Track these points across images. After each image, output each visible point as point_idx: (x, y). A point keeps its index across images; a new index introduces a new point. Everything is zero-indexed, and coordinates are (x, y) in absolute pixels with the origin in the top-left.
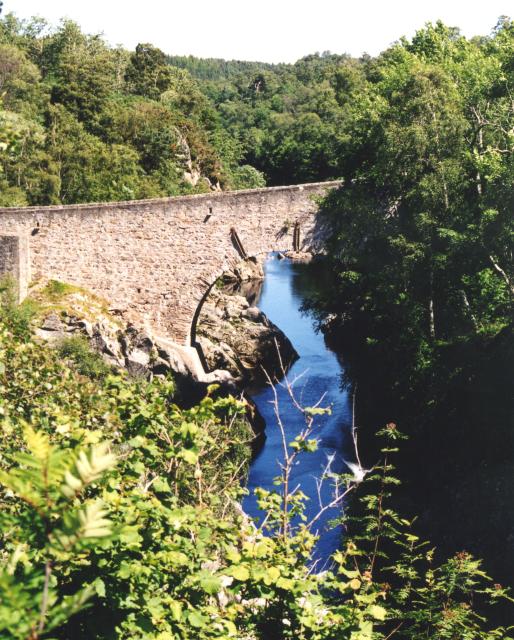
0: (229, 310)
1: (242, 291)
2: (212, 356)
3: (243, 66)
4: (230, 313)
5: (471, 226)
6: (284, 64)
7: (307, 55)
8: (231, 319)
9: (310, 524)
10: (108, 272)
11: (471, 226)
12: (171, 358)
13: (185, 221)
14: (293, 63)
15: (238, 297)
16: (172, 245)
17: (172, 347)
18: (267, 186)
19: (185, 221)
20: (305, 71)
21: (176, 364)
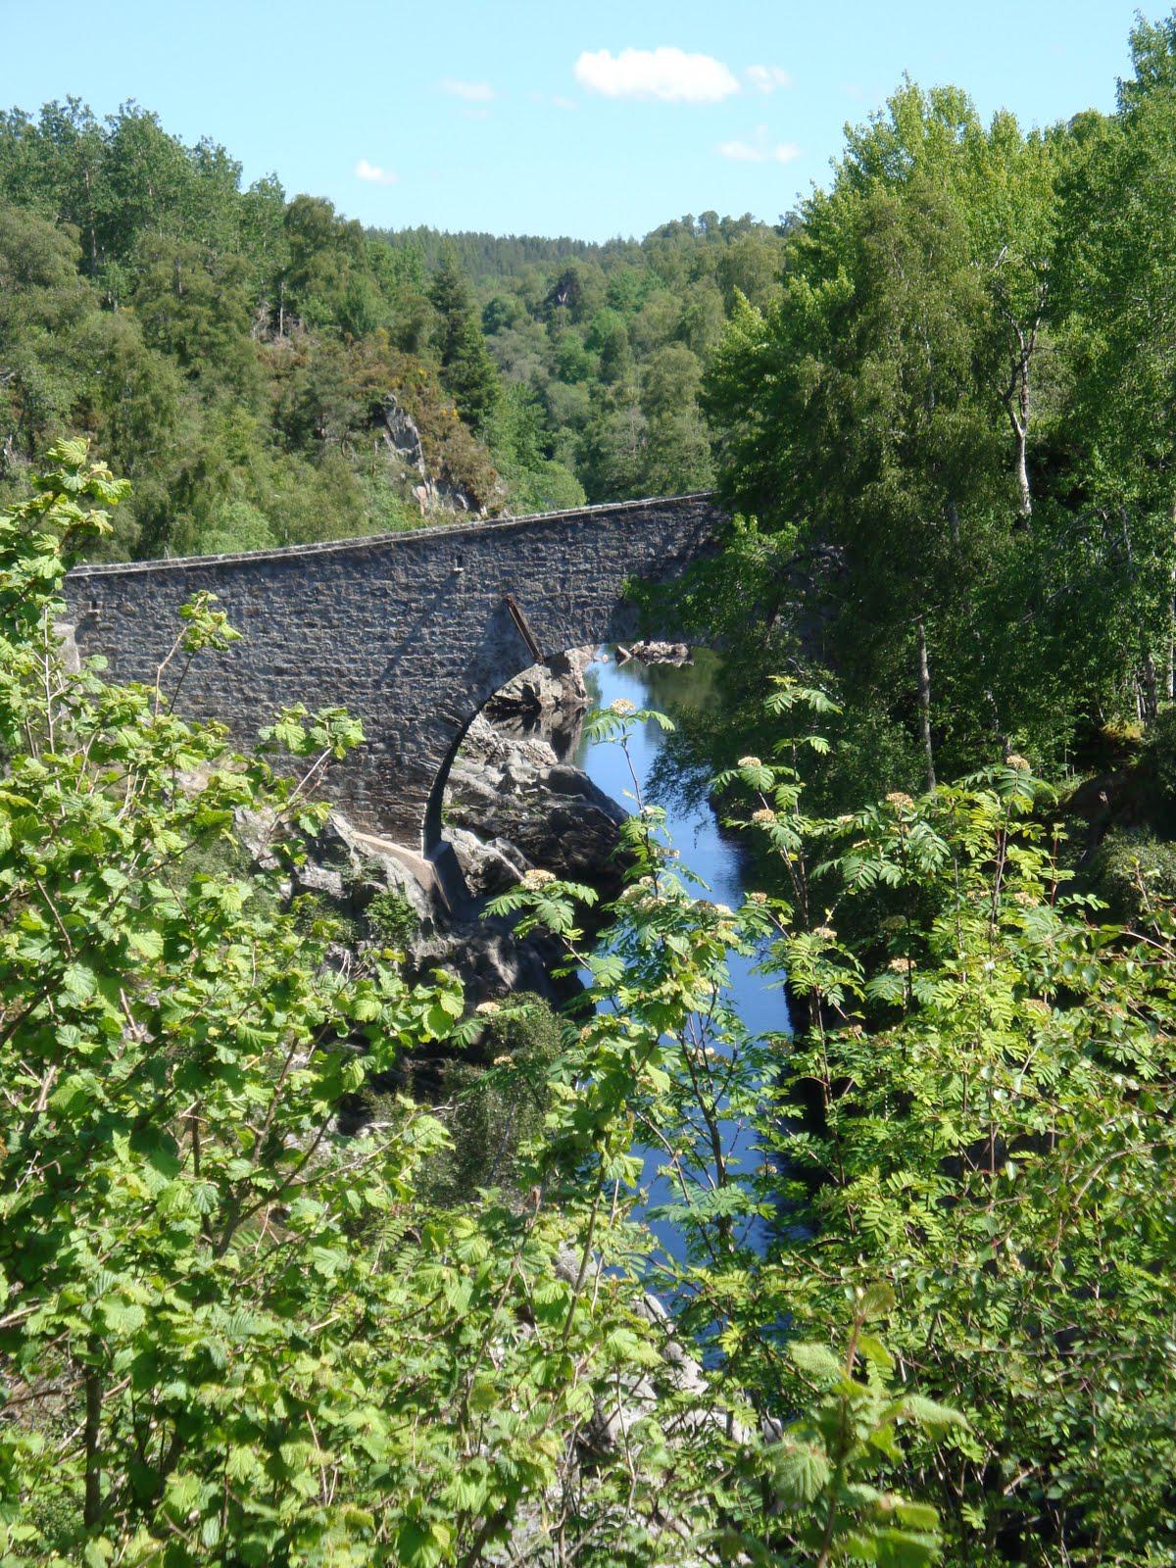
0: (512, 769)
1: (544, 729)
2: (479, 867)
3: (532, 247)
4: (515, 775)
5: (1089, 685)
6: (567, 240)
7: (666, 222)
8: (518, 790)
9: (865, 819)
10: (247, 700)
11: (1089, 685)
12: (392, 881)
13: (407, 588)
14: (601, 244)
15: (533, 741)
16: (382, 638)
17: (391, 853)
18: (590, 502)
19: (407, 588)
20: (406, 236)
21: (401, 887)
